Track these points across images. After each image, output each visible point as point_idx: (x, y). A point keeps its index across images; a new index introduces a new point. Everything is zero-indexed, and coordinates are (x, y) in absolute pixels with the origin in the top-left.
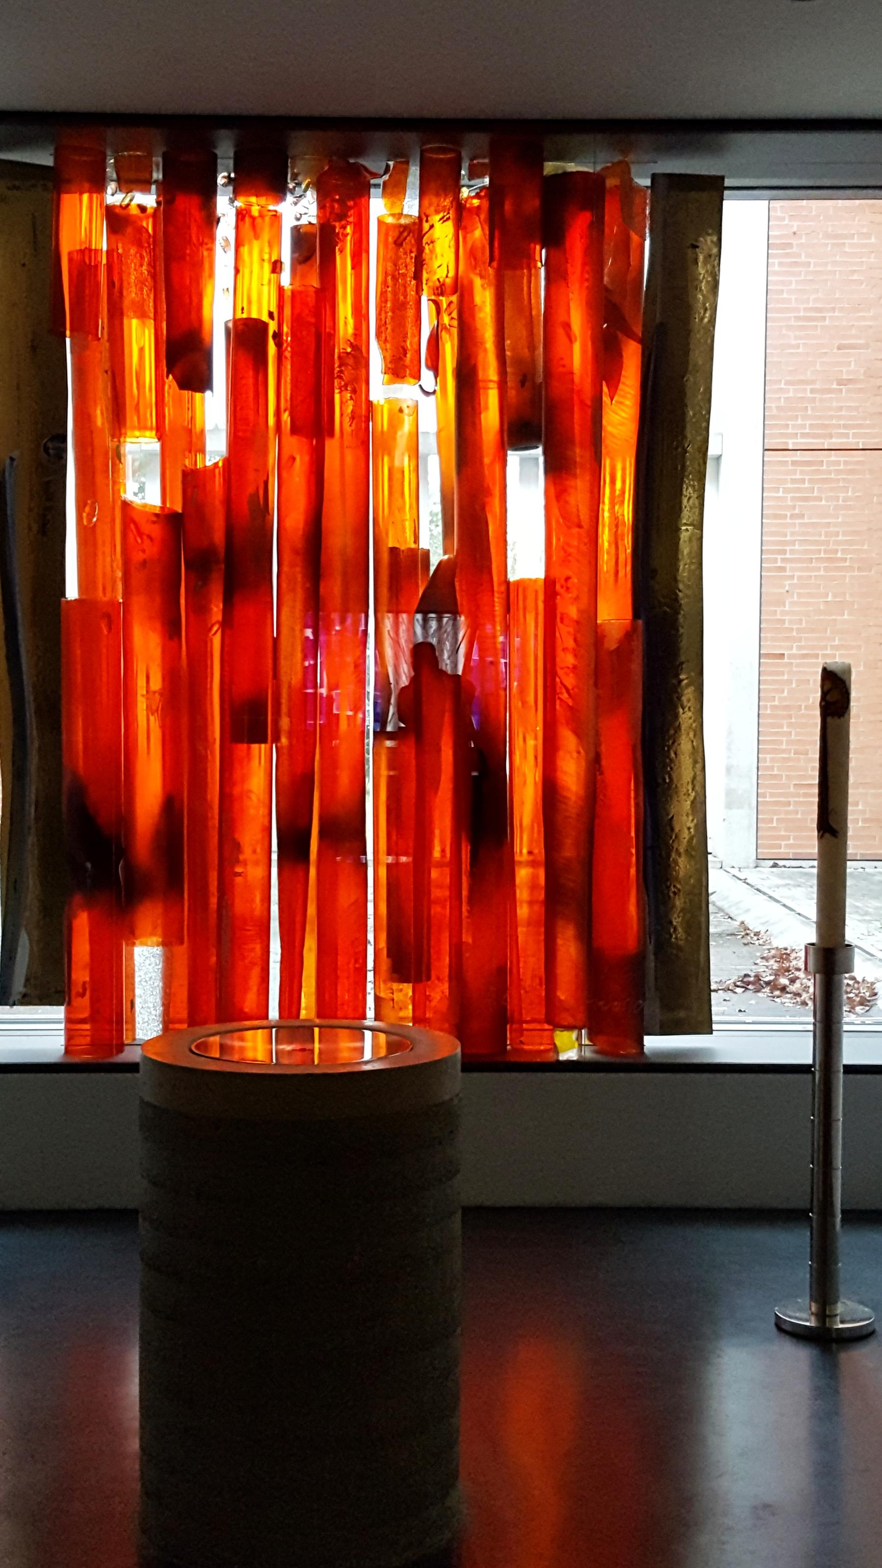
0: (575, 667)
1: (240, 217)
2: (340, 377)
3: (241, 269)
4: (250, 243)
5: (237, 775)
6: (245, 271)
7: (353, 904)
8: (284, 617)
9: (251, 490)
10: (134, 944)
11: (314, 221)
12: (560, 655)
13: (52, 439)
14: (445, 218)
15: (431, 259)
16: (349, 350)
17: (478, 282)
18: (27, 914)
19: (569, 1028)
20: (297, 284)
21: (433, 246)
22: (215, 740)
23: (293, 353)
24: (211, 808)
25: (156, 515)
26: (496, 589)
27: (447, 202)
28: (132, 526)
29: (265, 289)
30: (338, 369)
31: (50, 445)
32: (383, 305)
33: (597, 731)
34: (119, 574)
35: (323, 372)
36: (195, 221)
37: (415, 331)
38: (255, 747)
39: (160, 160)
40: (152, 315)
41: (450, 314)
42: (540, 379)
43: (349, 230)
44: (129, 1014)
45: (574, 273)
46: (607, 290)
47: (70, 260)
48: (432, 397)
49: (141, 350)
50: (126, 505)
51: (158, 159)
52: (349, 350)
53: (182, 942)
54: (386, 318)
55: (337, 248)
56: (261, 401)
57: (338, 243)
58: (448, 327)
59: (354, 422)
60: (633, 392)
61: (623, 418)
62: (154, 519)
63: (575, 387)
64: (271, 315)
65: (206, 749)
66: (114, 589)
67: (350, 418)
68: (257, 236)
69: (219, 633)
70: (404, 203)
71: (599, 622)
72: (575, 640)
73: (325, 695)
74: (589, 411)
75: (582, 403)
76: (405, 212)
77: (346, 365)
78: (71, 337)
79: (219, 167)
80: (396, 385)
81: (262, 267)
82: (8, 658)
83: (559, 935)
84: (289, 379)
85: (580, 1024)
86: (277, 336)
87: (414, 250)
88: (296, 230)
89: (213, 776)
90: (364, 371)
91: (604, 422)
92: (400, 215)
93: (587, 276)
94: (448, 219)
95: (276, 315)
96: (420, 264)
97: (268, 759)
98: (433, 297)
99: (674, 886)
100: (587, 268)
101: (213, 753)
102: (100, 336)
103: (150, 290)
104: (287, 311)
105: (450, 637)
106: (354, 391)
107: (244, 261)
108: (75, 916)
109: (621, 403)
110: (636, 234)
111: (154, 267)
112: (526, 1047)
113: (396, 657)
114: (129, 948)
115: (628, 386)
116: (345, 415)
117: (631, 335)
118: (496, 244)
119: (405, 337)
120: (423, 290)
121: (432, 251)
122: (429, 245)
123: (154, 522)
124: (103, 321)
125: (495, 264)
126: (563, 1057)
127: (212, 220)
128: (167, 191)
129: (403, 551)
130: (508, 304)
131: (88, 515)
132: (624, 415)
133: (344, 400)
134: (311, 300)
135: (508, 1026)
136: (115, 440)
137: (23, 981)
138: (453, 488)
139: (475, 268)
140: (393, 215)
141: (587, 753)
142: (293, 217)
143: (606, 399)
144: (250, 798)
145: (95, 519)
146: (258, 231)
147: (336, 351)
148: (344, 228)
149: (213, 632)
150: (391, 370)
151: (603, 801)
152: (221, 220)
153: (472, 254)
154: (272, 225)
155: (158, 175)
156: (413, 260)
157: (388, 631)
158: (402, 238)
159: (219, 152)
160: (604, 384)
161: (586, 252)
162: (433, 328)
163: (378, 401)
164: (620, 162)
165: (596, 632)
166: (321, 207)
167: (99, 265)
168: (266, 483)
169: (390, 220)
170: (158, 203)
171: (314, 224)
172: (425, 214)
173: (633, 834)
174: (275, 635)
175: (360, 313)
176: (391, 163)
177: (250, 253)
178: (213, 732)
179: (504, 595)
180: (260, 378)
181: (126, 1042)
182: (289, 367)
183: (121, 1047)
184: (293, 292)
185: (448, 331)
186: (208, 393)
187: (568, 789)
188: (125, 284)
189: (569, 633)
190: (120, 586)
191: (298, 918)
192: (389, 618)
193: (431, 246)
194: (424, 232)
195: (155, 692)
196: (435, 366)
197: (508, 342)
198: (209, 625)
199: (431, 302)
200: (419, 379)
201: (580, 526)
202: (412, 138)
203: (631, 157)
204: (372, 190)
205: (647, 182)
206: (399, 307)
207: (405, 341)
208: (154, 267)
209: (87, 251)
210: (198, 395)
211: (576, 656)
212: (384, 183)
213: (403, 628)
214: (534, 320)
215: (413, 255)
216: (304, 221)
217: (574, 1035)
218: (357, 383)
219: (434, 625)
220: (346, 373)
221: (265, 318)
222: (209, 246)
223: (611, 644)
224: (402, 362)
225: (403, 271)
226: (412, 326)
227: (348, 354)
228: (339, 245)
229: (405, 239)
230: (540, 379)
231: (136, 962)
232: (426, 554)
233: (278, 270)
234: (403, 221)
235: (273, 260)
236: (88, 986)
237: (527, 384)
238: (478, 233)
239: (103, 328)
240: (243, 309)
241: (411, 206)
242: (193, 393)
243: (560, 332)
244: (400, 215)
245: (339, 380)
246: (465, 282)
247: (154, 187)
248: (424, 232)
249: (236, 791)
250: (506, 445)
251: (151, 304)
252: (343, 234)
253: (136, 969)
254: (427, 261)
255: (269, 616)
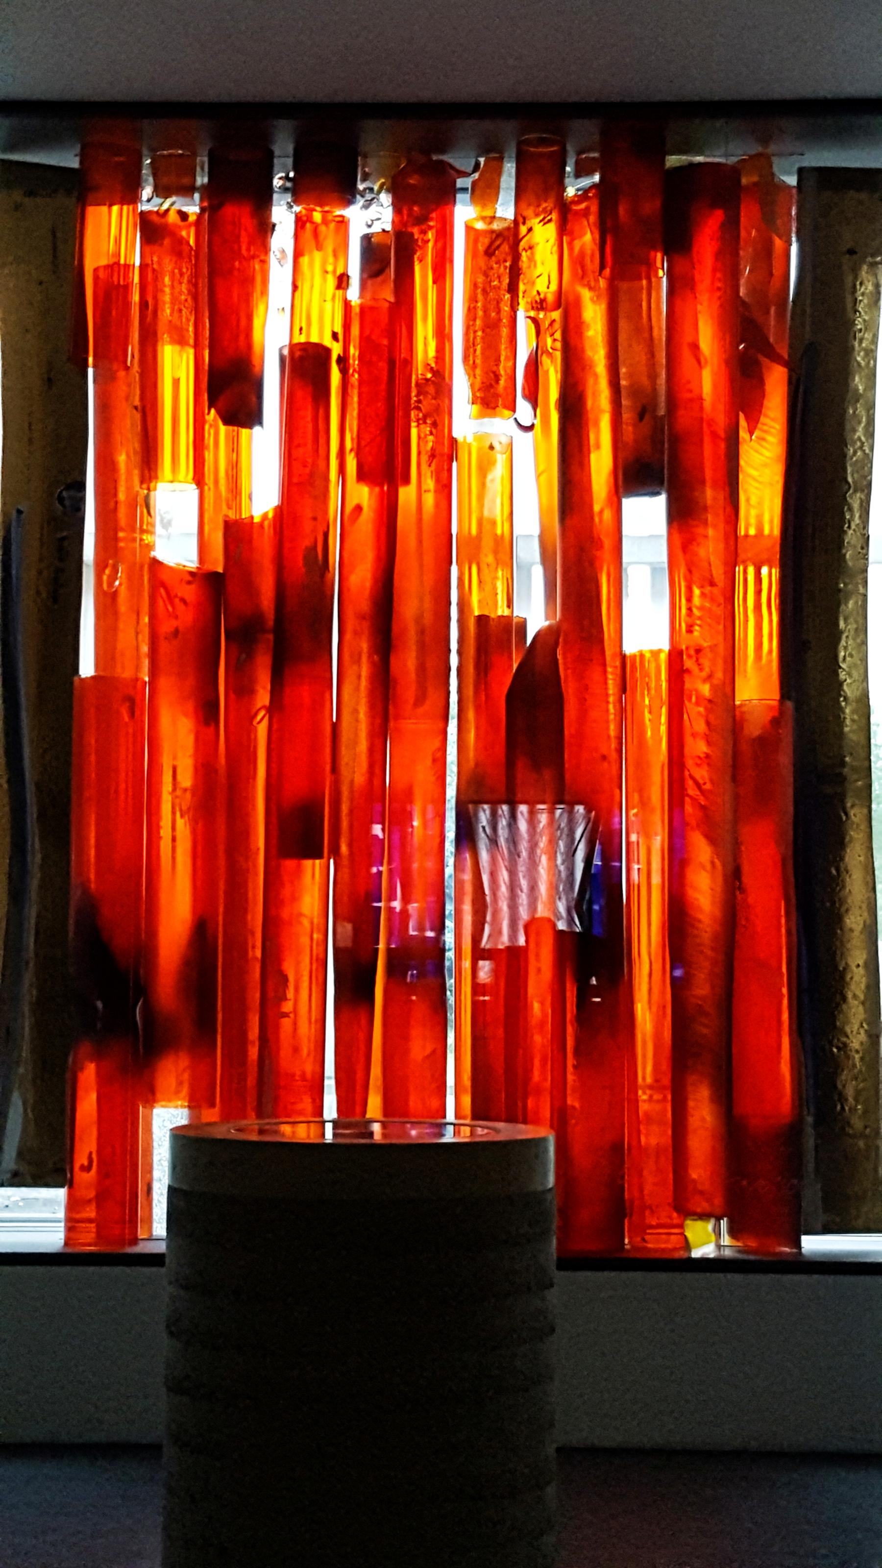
0: (707, 756)
1: (300, 223)
2: (418, 409)
3: (299, 284)
4: (311, 252)
5: (286, 892)
6: (304, 286)
7: (428, 1057)
8: (346, 697)
9: (307, 542)
10: (152, 1107)
11: (388, 227)
12: (689, 740)
13: (68, 487)
14: (546, 220)
15: (529, 267)
16: (429, 376)
17: (586, 294)
18: (21, 1070)
19: (703, 1216)
20: (368, 296)
21: (532, 254)
22: (258, 849)
23: (361, 381)
24: (253, 934)
25: (191, 574)
26: (608, 662)
27: (548, 205)
28: (162, 591)
29: (328, 305)
30: (415, 399)
31: (65, 494)
32: (471, 323)
33: (736, 839)
34: (145, 649)
35: (397, 382)
36: (246, 230)
37: (509, 354)
38: (308, 863)
39: (206, 159)
40: (192, 342)
41: (552, 335)
42: (662, 412)
43: (430, 235)
44: (145, 1203)
45: (702, 281)
46: (744, 303)
47: (96, 278)
48: (530, 435)
49: (176, 382)
50: (156, 563)
51: (203, 159)
52: (429, 376)
53: (213, 1105)
54: (475, 338)
55: (416, 257)
56: (322, 441)
57: (417, 251)
58: (551, 350)
59: (434, 461)
60: (778, 427)
61: (767, 457)
62: (190, 578)
63: (705, 416)
64: (335, 336)
65: (247, 859)
66: (138, 668)
67: (429, 457)
68: (319, 247)
69: (266, 720)
70: (497, 206)
71: (737, 703)
72: (708, 723)
73: (398, 910)
74: (723, 445)
75: (714, 435)
76: (498, 215)
77: (426, 394)
78: (94, 366)
79: (276, 169)
80: (486, 420)
81: (325, 280)
82: (7, 734)
83: (691, 1096)
84: (355, 413)
85: (718, 1211)
86: (343, 361)
87: (509, 258)
88: (367, 239)
89: (256, 888)
90: (447, 401)
91: (742, 463)
92: (493, 218)
93: (719, 285)
94: (550, 221)
95: (341, 337)
96: (515, 273)
97: (325, 874)
98: (532, 314)
99: (838, 1040)
100: (719, 275)
101: (255, 866)
102: (129, 364)
103: (191, 313)
104: (355, 331)
105: (564, 836)
106: (434, 425)
107: (303, 274)
108: (82, 1069)
109: (764, 439)
110: (780, 238)
111: (196, 285)
112: (650, 1246)
113: (493, 861)
114: (146, 1110)
115: (773, 420)
116: (423, 453)
117: (776, 358)
118: (608, 250)
119: (498, 360)
120: (518, 304)
121: (531, 259)
122: (526, 251)
123: (189, 583)
124: (133, 349)
125: (607, 271)
126: (696, 1254)
127: (267, 228)
128: (211, 209)
129: (493, 619)
130: (624, 325)
131: (109, 577)
132: (767, 454)
133: (422, 435)
134: (384, 319)
135: (626, 1221)
136: (145, 486)
137: (14, 1154)
138: (555, 540)
139: (583, 277)
140: (483, 218)
141: (724, 866)
142: (364, 223)
143: (743, 434)
144: (301, 923)
145: (117, 583)
146: (321, 238)
147: (414, 377)
148: (424, 232)
149: (259, 717)
150: (479, 400)
151: (745, 926)
152: (277, 228)
153: (579, 262)
154: (337, 230)
155: (202, 180)
156: (508, 271)
157: (484, 828)
158: (493, 247)
159: (277, 150)
160: (742, 416)
161: (718, 255)
162: (532, 350)
163: (465, 438)
164: (759, 155)
165: (734, 717)
166: (397, 207)
167: (131, 285)
168: (326, 535)
169: (480, 226)
170: (203, 210)
171: (388, 232)
172: (521, 215)
173: (784, 970)
174: (334, 720)
175: (443, 334)
176: (482, 160)
177: (311, 265)
178: (257, 842)
179: (619, 671)
180: (321, 412)
181: (140, 1237)
182: (356, 399)
183: (135, 1241)
184: (362, 307)
185: (550, 355)
186: (257, 429)
187: (699, 909)
188: (160, 303)
189: (699, 713)
190: (146, 663)
191: (360, 1075)
192: (484, 811)
193: (529, 252)
194: (521, 236)
195: (185, 790)
196: (533, 396)
197: (623, 370)
198: (254, 710)
199: (529, 321)
200: (514, 411)
201: (712, 584)
202: (508, 128)
203: (772, 148)
204: (459, 196)
205: (792, 180)
206: (491, 327)
207: (498, 365)
208: (196, 285)
209: (116, 268)
210: (244, 432)
211: (709, 743)
212: (474, 184)
213: (503, 823)
214: (656, 342)
215: (508, 264)
216: (377, 228)
217: (710, 1226)
218: (438, 415)
219: (543, 819)
220: (425, 403)
221: (328, 341)
222: (262, 257)
223: (754, 728)
224: (492, 391)
225: (495, 283)
226: (506, 348)
227: (427, 380)
228: (418, 254)
229: (498, 247)
230: (662, 412)
231: (154, 1136)
232: (522, 627)
233: (344, 285)
234: (495, 226)
235: (338, 273)
236: (94, 1156)
237: (647, 418)
238: (588, 237)
239: (133, 356)
240: (301, 329)
241: (505, 209)
242: (240, 429)
243: (686, 355)
244: (493, 218)
245: (416, 412)
246: (571, 298)
247: (197, 196)
248: (521, 236)
249: (285, 914)
250: (621, 490)
251: (191, 329)
252: (423, 240)
253: (155, 1144)
254: (524, 270)
255: (327, 695)
